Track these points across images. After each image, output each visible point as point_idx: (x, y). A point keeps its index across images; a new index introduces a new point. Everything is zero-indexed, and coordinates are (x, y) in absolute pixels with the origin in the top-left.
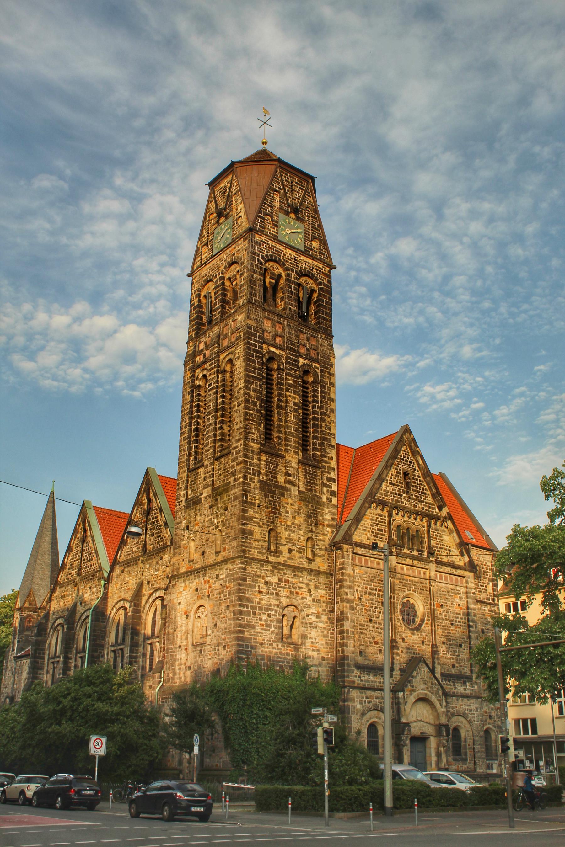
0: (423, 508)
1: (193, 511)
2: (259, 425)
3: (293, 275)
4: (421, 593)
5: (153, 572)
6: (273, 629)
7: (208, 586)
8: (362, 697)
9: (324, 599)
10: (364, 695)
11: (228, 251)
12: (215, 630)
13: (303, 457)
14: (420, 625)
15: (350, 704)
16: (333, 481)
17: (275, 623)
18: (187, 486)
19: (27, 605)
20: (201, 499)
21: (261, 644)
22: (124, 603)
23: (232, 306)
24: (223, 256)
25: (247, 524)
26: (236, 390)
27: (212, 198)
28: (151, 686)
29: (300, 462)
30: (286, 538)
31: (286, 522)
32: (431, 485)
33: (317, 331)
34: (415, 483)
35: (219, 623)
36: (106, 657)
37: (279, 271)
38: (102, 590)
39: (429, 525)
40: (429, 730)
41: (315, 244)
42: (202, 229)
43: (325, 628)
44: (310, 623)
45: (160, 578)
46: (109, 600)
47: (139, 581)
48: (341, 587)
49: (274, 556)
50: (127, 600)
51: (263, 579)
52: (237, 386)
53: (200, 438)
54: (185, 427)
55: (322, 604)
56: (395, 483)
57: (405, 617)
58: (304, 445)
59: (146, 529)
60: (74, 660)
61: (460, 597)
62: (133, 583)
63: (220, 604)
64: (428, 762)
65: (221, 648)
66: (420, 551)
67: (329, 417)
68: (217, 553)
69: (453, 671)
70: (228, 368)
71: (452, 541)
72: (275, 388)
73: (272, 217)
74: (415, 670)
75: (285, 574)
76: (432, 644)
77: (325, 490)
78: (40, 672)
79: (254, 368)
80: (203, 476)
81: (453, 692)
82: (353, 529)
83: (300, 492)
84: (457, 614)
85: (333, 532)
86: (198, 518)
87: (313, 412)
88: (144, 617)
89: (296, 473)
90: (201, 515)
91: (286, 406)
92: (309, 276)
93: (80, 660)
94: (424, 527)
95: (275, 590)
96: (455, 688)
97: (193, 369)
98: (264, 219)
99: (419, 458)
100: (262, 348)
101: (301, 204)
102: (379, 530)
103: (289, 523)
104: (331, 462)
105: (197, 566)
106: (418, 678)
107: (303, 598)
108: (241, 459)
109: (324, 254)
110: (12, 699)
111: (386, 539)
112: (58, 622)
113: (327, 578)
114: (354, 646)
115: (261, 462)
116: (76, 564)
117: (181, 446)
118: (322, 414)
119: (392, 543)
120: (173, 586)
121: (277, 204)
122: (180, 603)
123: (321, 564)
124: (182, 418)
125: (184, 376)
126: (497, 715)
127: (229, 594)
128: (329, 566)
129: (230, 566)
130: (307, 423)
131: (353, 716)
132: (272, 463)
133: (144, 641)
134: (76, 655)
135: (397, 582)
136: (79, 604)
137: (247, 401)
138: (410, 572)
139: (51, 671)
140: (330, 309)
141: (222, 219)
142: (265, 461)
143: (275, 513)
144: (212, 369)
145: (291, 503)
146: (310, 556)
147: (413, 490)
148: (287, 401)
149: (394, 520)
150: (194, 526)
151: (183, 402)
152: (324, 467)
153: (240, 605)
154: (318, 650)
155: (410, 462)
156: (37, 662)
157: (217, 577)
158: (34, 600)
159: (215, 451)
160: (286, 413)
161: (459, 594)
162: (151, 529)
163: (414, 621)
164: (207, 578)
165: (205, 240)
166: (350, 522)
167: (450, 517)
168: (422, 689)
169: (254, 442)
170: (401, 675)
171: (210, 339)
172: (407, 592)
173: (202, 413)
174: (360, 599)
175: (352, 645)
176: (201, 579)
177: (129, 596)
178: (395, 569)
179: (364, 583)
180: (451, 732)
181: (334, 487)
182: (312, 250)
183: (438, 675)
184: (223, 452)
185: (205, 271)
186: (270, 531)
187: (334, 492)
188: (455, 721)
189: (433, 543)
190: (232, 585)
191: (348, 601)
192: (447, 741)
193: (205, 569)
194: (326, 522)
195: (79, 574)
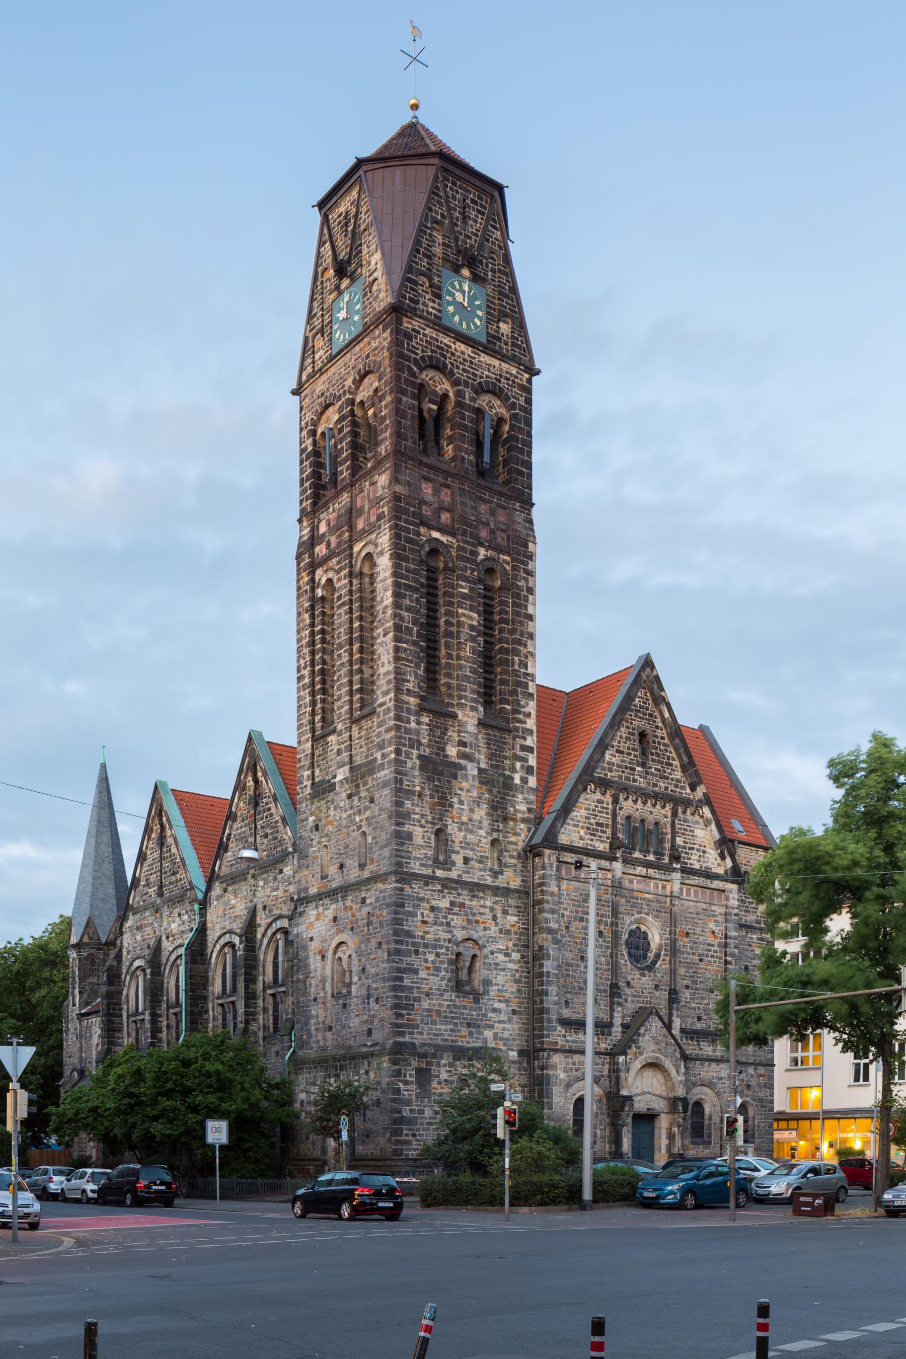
0: (666, 789)
1: (324, 801)
2: (418, 666)
3: (468, 393)
4: (657, 917)
5: (270, 893)
6: (443, 973)
7: (350, 913)
8: (568, 1064)
9: (516, 929)
10: (570, 1060)
11: (357, 348)
12: (363, 977)
13: (484, 716)
14: (654, 963)
15: (550, 1072)
16: (530, 750)
17: (446, 966)
18: (312, 764)
19: (86, 939)
20: (334, 784)
21: (427, 994)
22: (231, 937)
23: (369, 455)
24: (350, 358)
25: (404, 824)
26: (379, 608)
27: (327, 235)
28: (277, 1053)
29: (481, 724)
30: (461, 842)
31: (459, 818)
32: (682, 750)
33: (509, 498)
34: (656, 748)
35: (368, 967)
36: (211, 1013)
37: (444, 386)
38: (197, 917)
39: (675, 814)
40: (659, 1105)
41: (505, 328)
42: (312, 300)
43: (517, 971)
44: (496, 964)
45: (280, 900)
46: (208, 932)
47: (250, 904)
48: (541, 911)
49: (444, 870)
50: (235, 933)
51: (428, 903)
52: (382, 601)
53: (327, 686)
54: (305, 668)
55: (513, 935)
56: (626, 750)
57: (633, 951)
58: (487, 696)
59: (256, 827)
60: (165, 1018)
61: (715, 921)
62: (240, 907)
63: (369, 940)
64: (656, 1146)
65: (372, 1004)
66: (659, 854)
67: (526, 646)
68: (362, 866)
69: (699, 1026)
70: (366, 570)
71: (709, 837)
72: (441, 602)
73: (430, 279)
74: (642, 1025)
75: (459, 894)
76: (670, 990)
77: (518, 765)
78: (117, 1034)
79: (408, 570)
80: (336, 748)
81: (697, 1055)
82: (559, 825)
83: (480, 769)
84: (709, 945)
85: (529, 830)
86: (332, 812)
87: (501, 640)
88: (262, 957)
89: (474, 742)
90: (335, 809)
91: (458, 632)
92: (493, 393)
93: (173, 1018)
94: (666, 817)
95: (446, 918)
96: (700, 1049)
97: (313, 567)
98: (415, 283)
99: (665, 709)
100: (418, 534)
101: (481, 247)
102: (598, 824)
103: (465, 819)
104: (528, 721)
105: (334, 885)
106: (647, 1037)
107: (485, 929)
108: (392, 723)
109: (519, 347)
110: (82, 1073)
111: (608, 838)
112: (137, 963)
113: (520, 898)
114: (558, 995)
115: (420, 725)
116: (153, 878)
117: (299, 698)
118: (514, 642)
119: (617, 843)
120: (301, 914)
121: (438, 250)
122: (311, 939)
123: (511, 879)
124: (298, 652)
125: (298, 581)
126: (758, 1084)
127: (381, 926)
128: (522, 881)
129: (380, 885)
130: (491, 658)
131: (554, 1088)
132: (437, 727)
133: (264, 991)
134: (168, 1011)
135: (623, 901)
136: (164, 938)
137: (397, 628)
138: (641, 887)
139: (134, 1034)
140: (529, 454)
141: (346, 282)
142: (427, 724)
143: (443, 805)
144: (341, 569)
145: (467, 790)
146: (496, 868)
147: (653, 760)
148: (460, 624)
149: (621, 809)
150: (325, 826)
151: (298, 625)
152: (517, 729)
153: (397, 942)
154: (507, 1001)
155: (651, 715)
156: (113, 1022)
157: (363, 901)
158: (96, 932)
159: (351, 709)
160: (459, 643)
161: (714, 916)
162: (262, 827)
163: (645, 957)
164: (348, 903)
165: (317, 322)
166: (555, 814)
167: (707, 800)
168: (652, 1052)
169: (410, 696)
170: (623, 1032)
171: (335, 515)
172: (637, 916)
173: (329, 643)
174: (567, 928)
175: (554, 993)
176: (341, 904)
177: (237, 926)
178: (620, 883)
179: (574, 905)
180: (690, 1108)
181: (532, 761)
182: (500, 340)
183: (676, 1032)
184: (364, 710)
185: (320, 385)
186: (438, 832)
187: (532, 767)
188: (699, 1093)
189: (679, 841)
190: (385, 912)
191: (550, 931)
192: (684, 1119)
193: (344, 890)
194: (519, 815)
195: (160, 894)
